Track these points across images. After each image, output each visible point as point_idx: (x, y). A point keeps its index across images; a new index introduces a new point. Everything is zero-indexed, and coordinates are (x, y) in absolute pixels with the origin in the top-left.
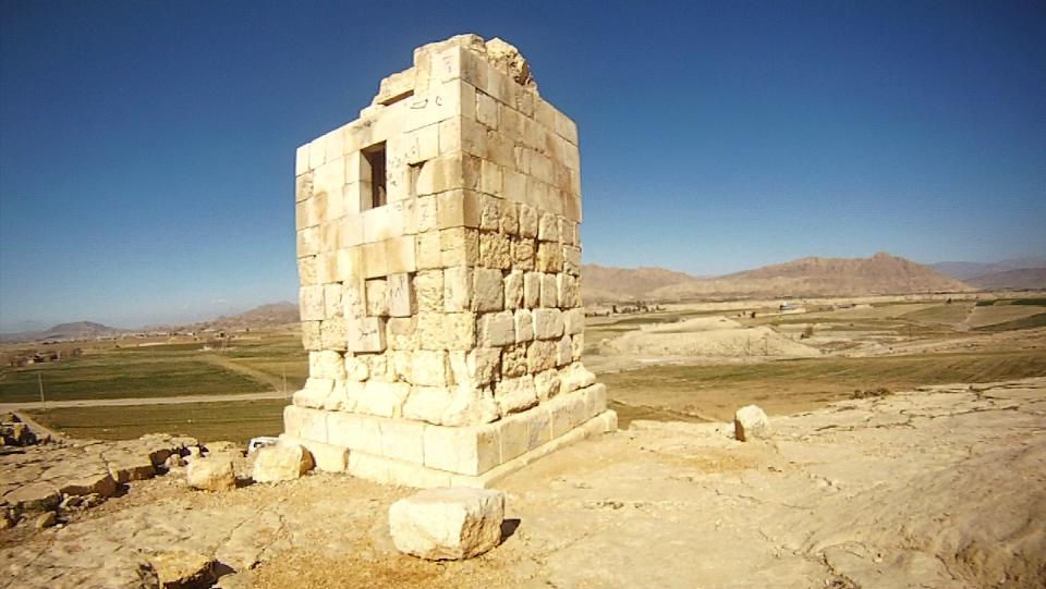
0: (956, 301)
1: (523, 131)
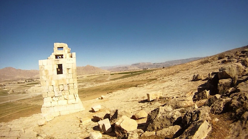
0: (106, 74)
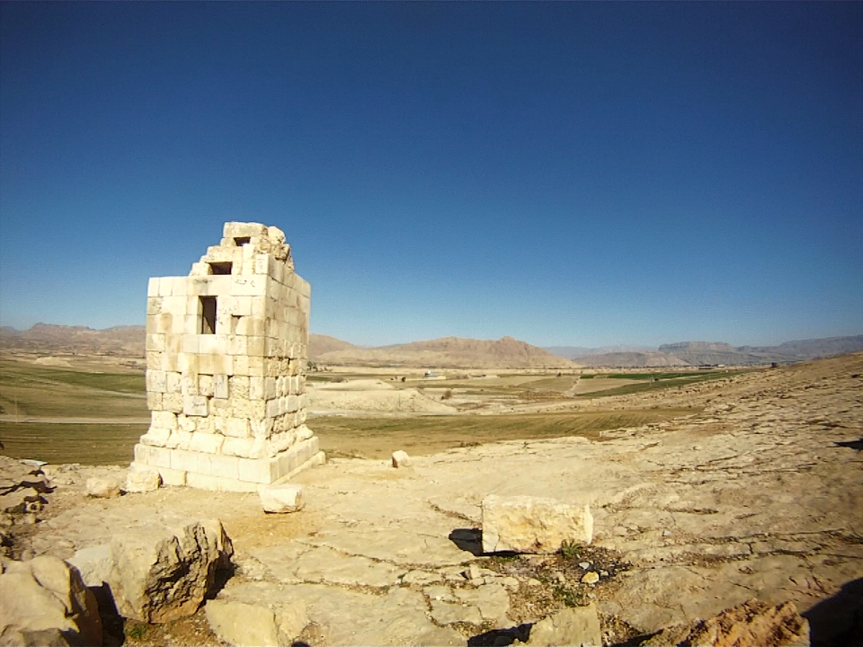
0: (564, 374)
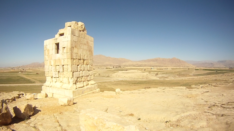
0: (190, 69)
1: (82, 41)
